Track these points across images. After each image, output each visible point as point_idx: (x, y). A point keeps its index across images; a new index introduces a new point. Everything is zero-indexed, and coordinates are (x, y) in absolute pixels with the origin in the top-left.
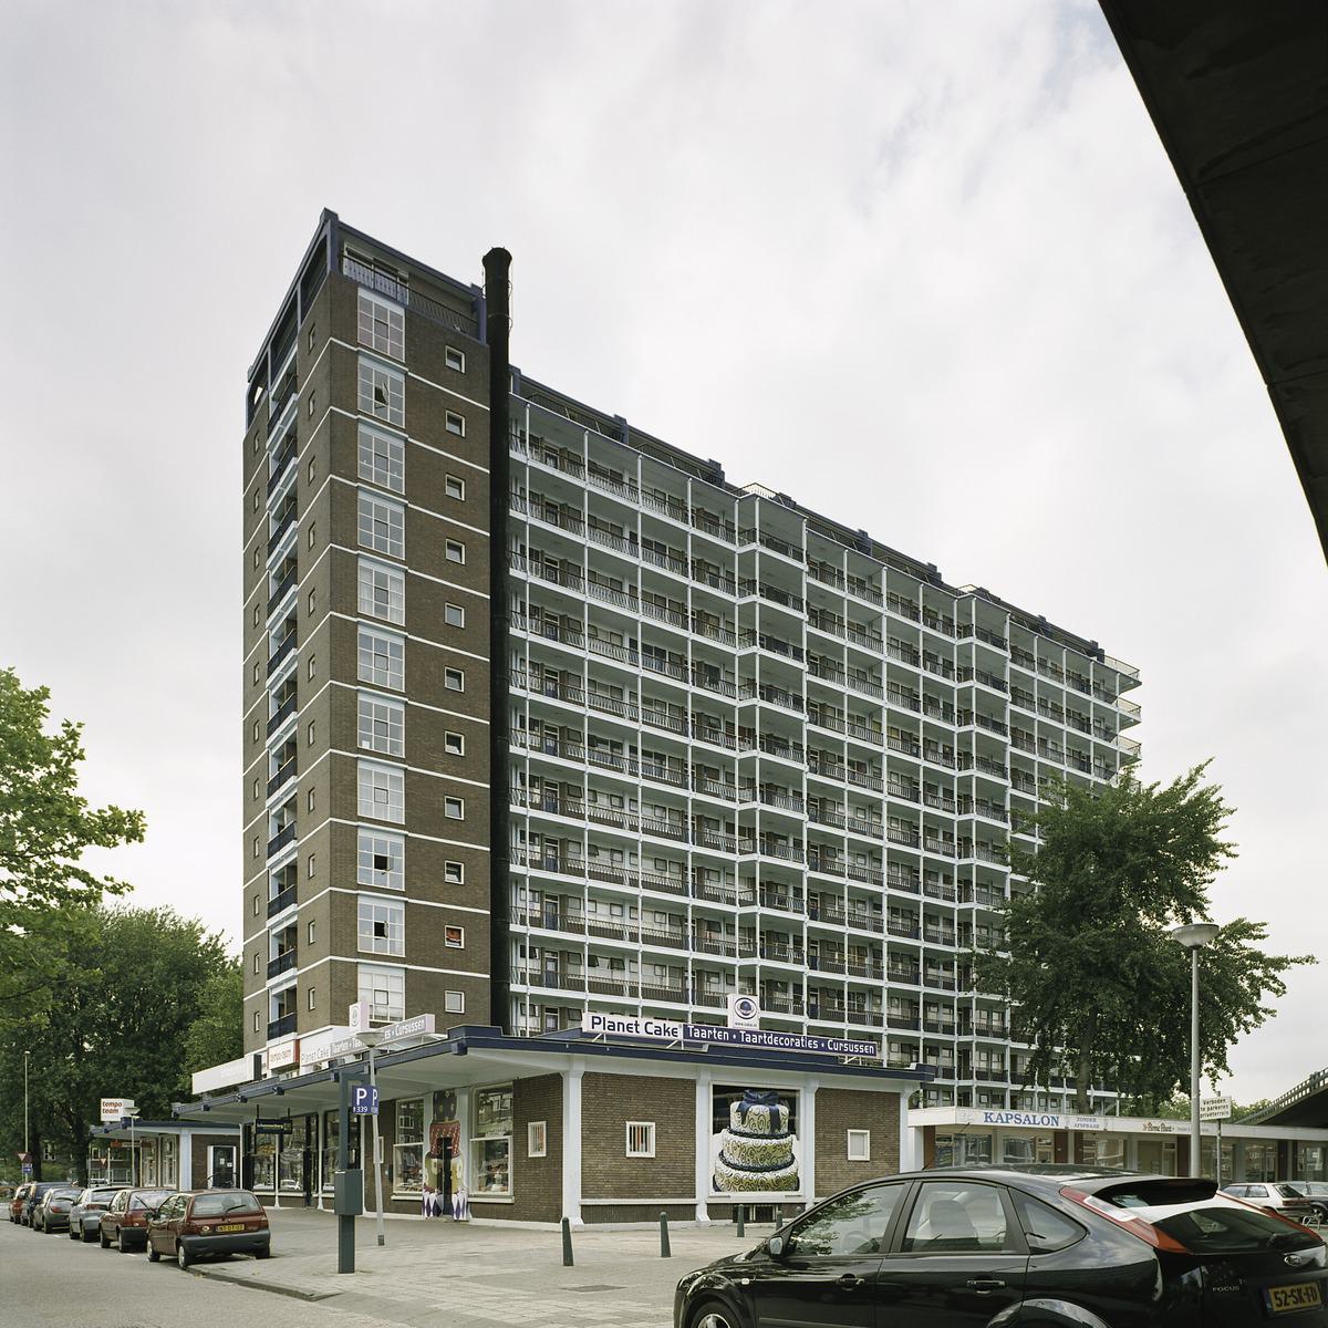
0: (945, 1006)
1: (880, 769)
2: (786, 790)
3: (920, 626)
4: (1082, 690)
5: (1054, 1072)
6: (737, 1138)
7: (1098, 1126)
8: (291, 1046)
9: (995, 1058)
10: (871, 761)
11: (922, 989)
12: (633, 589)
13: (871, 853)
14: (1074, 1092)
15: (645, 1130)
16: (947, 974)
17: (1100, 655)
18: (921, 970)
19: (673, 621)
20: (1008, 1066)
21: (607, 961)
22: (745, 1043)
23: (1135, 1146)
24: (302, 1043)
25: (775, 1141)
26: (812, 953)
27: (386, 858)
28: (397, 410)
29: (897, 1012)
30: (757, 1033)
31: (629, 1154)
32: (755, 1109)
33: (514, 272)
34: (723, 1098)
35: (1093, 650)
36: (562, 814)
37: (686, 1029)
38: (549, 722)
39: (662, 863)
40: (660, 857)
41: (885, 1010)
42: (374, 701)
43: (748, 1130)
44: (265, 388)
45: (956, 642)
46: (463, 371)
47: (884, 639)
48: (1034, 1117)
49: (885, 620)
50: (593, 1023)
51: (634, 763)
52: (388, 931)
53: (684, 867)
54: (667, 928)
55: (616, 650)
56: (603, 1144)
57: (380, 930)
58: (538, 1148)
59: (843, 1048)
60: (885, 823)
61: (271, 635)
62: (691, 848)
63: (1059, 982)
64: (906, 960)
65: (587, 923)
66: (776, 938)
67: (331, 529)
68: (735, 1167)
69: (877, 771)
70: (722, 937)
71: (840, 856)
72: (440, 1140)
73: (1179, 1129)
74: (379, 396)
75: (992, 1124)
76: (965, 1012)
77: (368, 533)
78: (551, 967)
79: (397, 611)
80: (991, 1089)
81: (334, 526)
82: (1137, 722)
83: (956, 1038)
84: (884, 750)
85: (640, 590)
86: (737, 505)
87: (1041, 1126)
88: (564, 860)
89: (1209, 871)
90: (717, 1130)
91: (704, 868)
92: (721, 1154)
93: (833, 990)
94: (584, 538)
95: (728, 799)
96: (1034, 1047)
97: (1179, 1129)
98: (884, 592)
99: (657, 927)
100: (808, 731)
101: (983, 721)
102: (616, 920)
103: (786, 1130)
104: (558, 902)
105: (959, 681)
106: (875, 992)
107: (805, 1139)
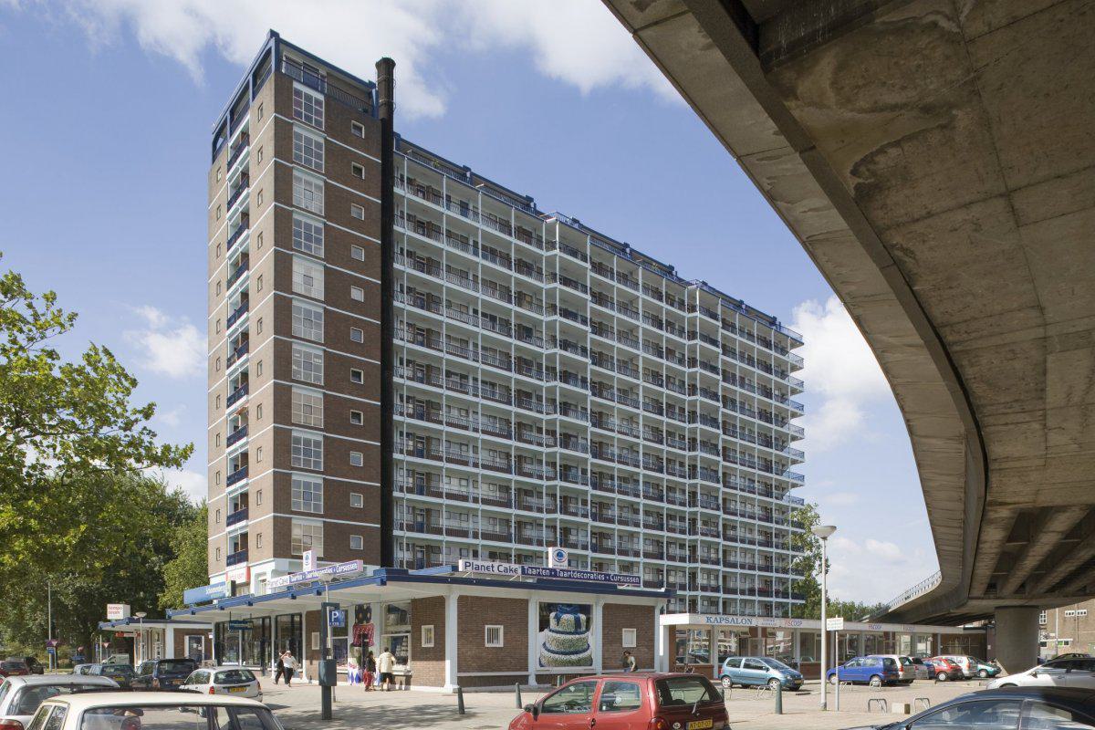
3: (663, 304)
4: (767, 347)
6: (554, 635)
8: (244, 571)
9: (712, 577)
18: (665, 522)
19: (502, 298)
20: (721, 583)
22: (559, 577)
24: (252, 569)
25: (577, 636)
29: (650, 549)
30: (567, 571)
31: (487, 645)
32: (565, 617)
38: (419, 361)
43: (560, 629)
44: (225, 139)
47: (640, 312)
51: (476, 388)
55: (464, 316)
65: (445, 491)
72: (359, 636)
78: (419, 519)
79: (318, 290)
80: (710, 597)
84: (640, 382)
85: (480, 278)
88: (429, 451)
90: (541, 629)
92: (544, 644)
94: (443, 245)
95: (538, 412)
98: (640, 282)
99: (491, 494)
100: (591, 370)
102: (463, 489)
105: (689, 395)
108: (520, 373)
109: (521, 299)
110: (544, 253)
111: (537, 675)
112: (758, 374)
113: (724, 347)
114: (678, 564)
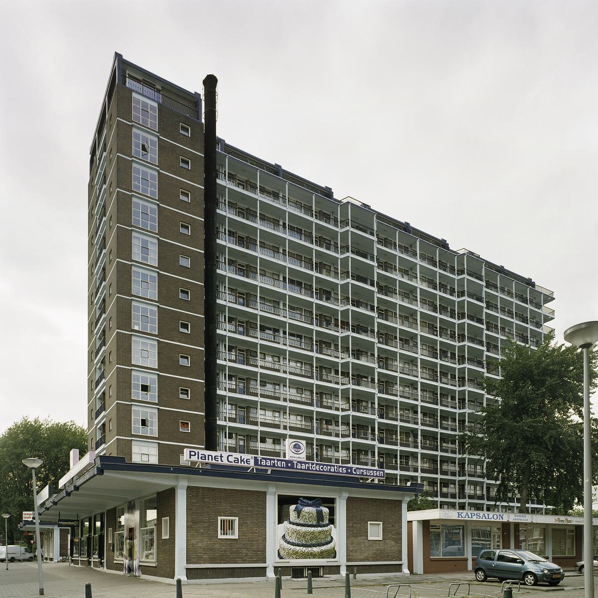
0: (452, 463)
1: (417, 343)
2: (367, 353)
4: (524, 302)
5: (510, 495)
6: (295, 527)
7: (527, 520)
10: (412, 338)
11: (439, 453)
12: (284, 251)
13: (412, 385)
14: (519, 505)
15: (232, 523)
16: (453, 446)
17: (533, 285)
20: (485, 493)
21: (271, 440)
22: (297, 469)
23: (550, 532)
25: (320, 529)
26: (381, 435)
27: (147, 386)
28: (153, 155)
29: (426, 465)
30: (305, 463)
32: (306, 509)
33: (219, 89)
34: (284, 502)
35: (530, 283)
36: (247, 365)
37: (256, 460)
39: (301, 390)
40: (300, 387)
41: (419, 464)
42: (141, 305)
43: (302, 522)
45: (456, 277)
46: (190, 136)
48: (488, 515)
49: (418, 266)
50: (190, 455)
52: (149, 423)
53: (312, 392)
54: (303, 423)
56: (202, 531)
57: (144, 423)
58: (166, 534)
59: (363, 473)
60: (419, 370)
61: (97, 278)
62: (315, 382)
63: (510, 449)
64: (431, 439)
65: (259, 420)
66: (361, 427)
67: (117, 217)
68: (293, 544)
69: (415, 343)
70: (331, 428)
71: (396, 387)
73: (576, 522)
74: (144, 148)
75: (462, 519)
76: (462, 465)
77: (137, 218)
79: (153, 259)
81: (119, 215)
82: (553, 319)
83: (457, 478)
86: (339, 208)
87: (492, 520)
89: (592, 388)
90: (280, 521)
91: (323, 393)
92: (284, 537)
93: (391, 454)
94: (258, 225)
95: (336, 357)
96: (498, 482)
97: (576, 522)
101: (471, 318)
102: (276, 419)
103: (327, 522)
104: (245, 409)
106: (414, 455)
107: (340, 525)
108: (321, 326)
109: (320, 267)
111: (275, 567)
113: (487, 303)
114: (449, 477)
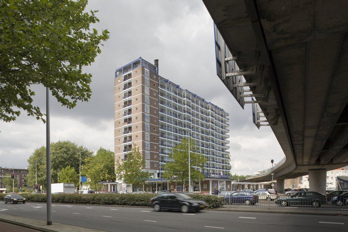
110: (183, 99)
112: (173, 102)
